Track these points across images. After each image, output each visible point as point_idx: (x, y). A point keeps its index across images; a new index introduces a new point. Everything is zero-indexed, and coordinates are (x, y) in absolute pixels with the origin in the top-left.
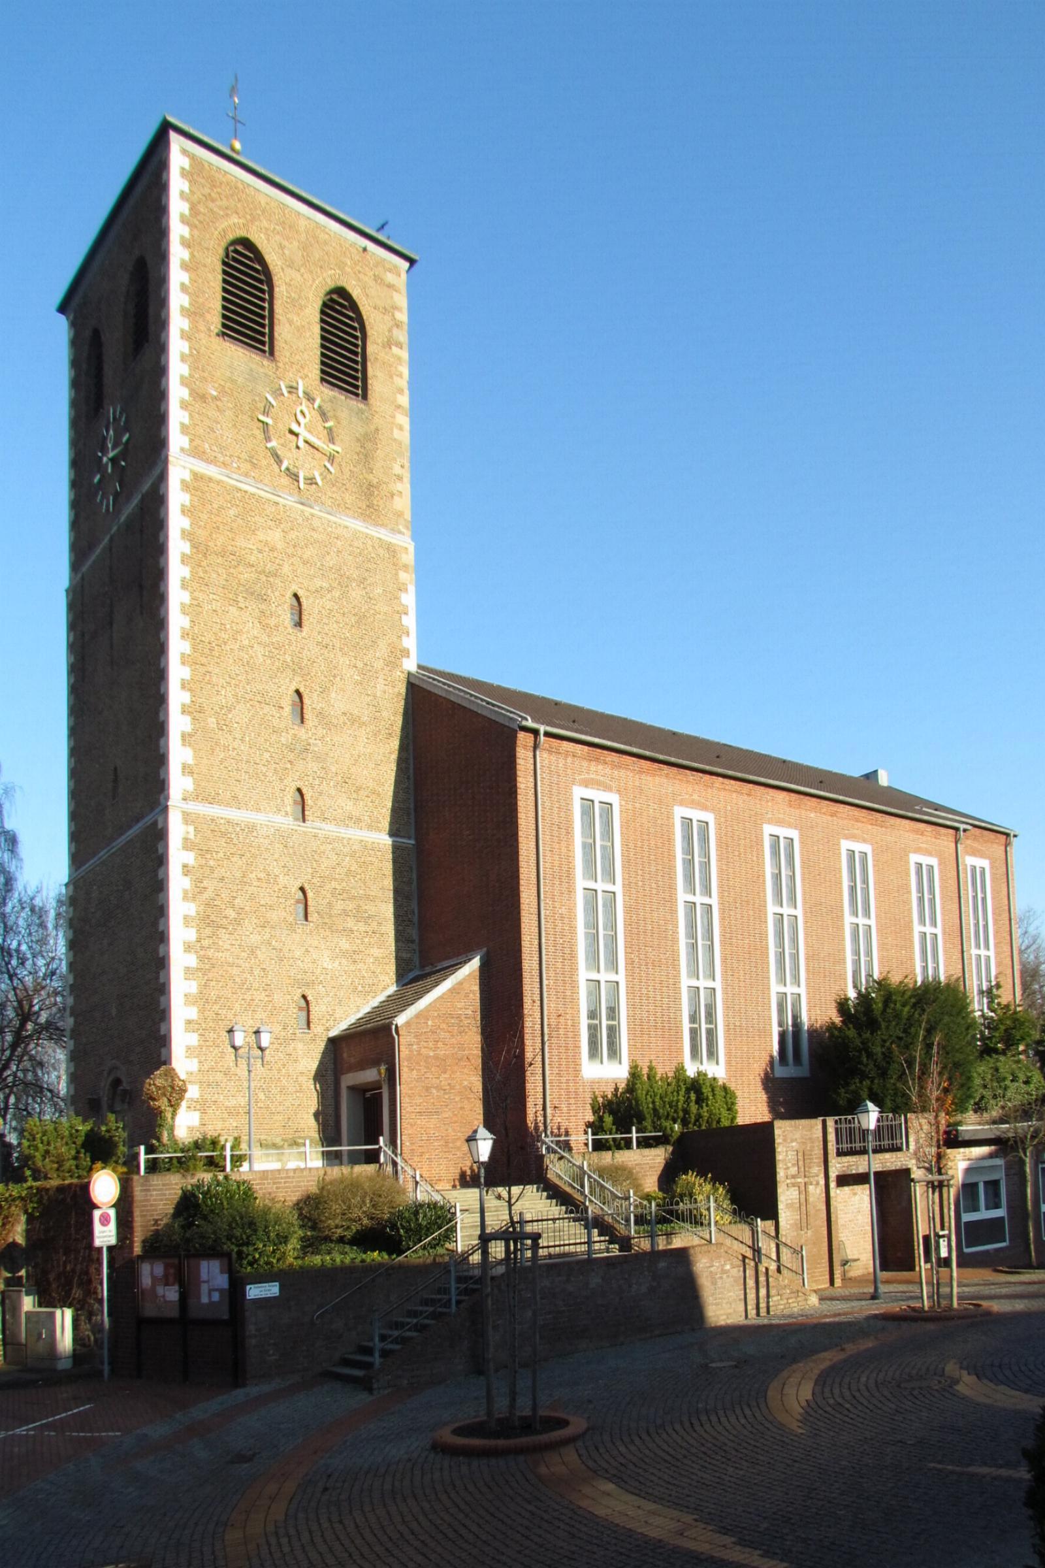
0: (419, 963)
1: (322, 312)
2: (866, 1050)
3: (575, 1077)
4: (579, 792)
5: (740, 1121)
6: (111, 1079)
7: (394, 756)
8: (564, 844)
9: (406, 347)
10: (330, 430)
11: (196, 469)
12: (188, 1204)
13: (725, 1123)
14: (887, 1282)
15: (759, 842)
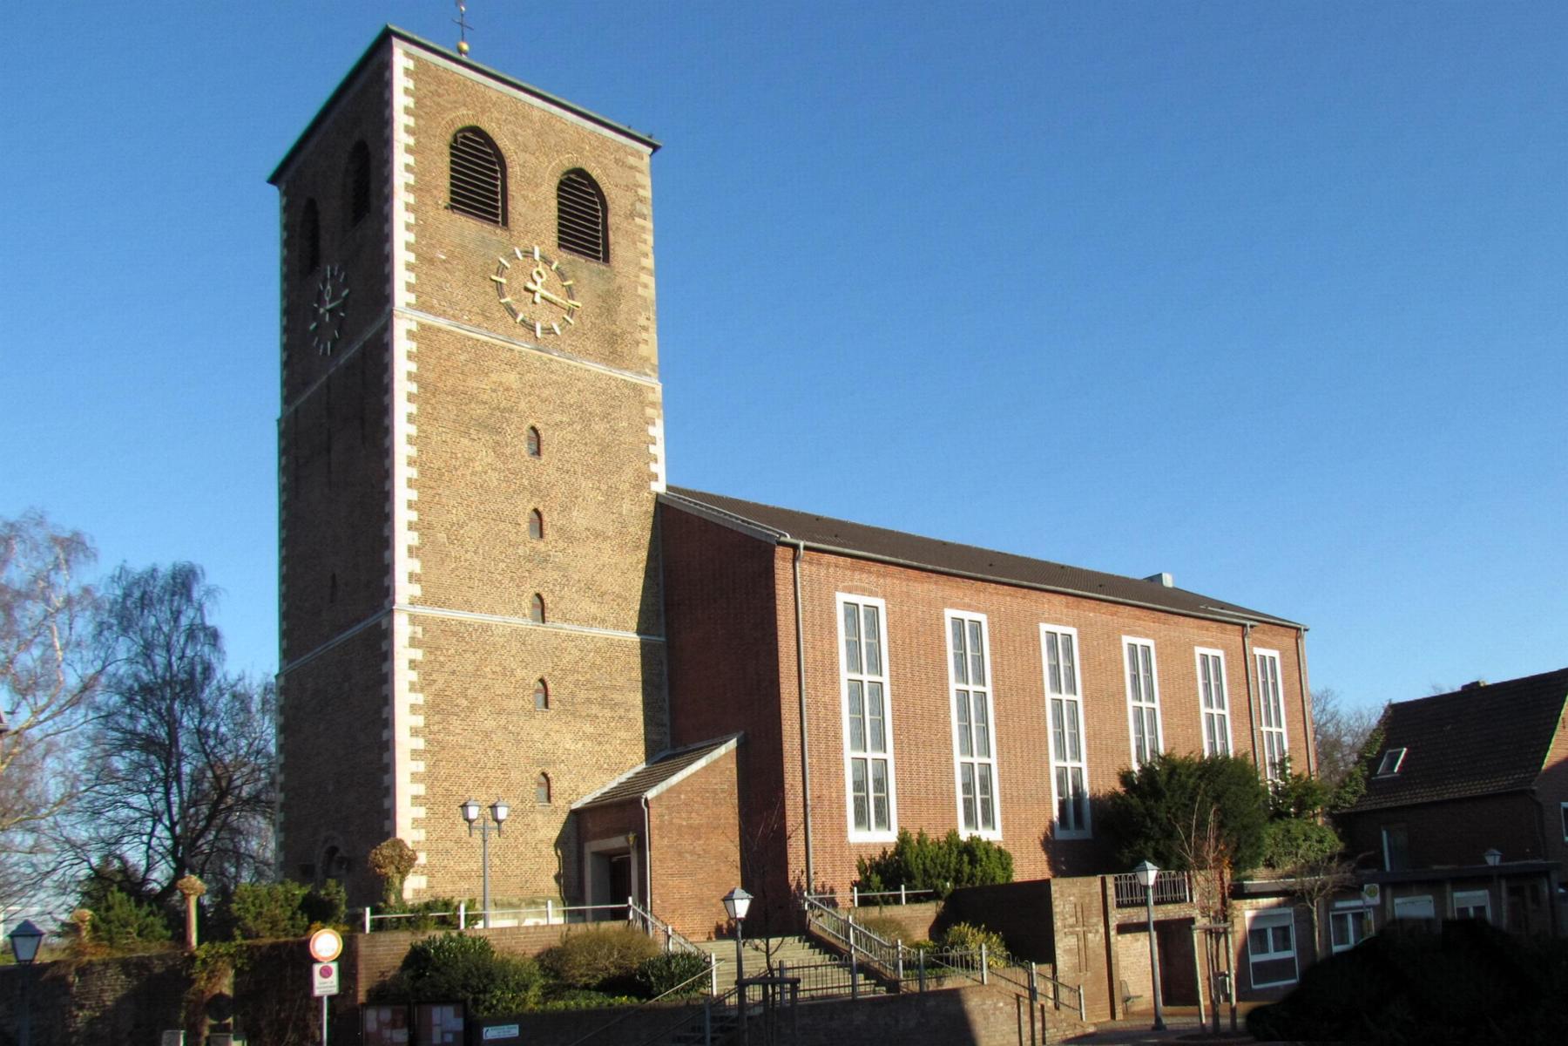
0: (670, 739)
1: (559, 189)
2: (1150, 815)
3: (841, 838)
4: (841, 598)
5: (1017, 877)
6: (328, 846)
7: (642, 565)
8: (826, 642)
9: (650, 218)
10: (569, 287)
11: (425, 321)
12: (417, 959)
13: (1000, 880)
14: (1172, 1015)
15: (1037, 638)
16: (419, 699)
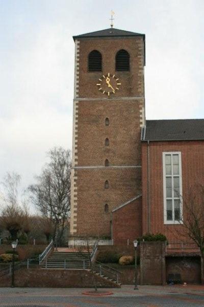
15: (177, 151)
16: (76, 188)
